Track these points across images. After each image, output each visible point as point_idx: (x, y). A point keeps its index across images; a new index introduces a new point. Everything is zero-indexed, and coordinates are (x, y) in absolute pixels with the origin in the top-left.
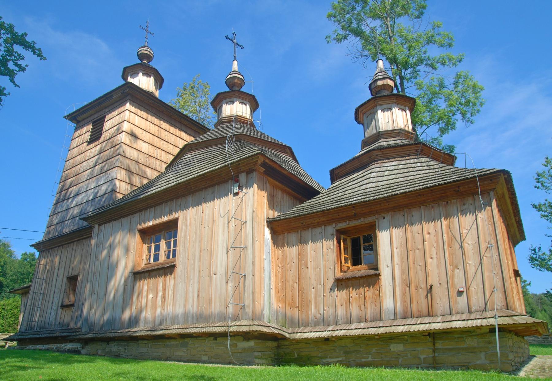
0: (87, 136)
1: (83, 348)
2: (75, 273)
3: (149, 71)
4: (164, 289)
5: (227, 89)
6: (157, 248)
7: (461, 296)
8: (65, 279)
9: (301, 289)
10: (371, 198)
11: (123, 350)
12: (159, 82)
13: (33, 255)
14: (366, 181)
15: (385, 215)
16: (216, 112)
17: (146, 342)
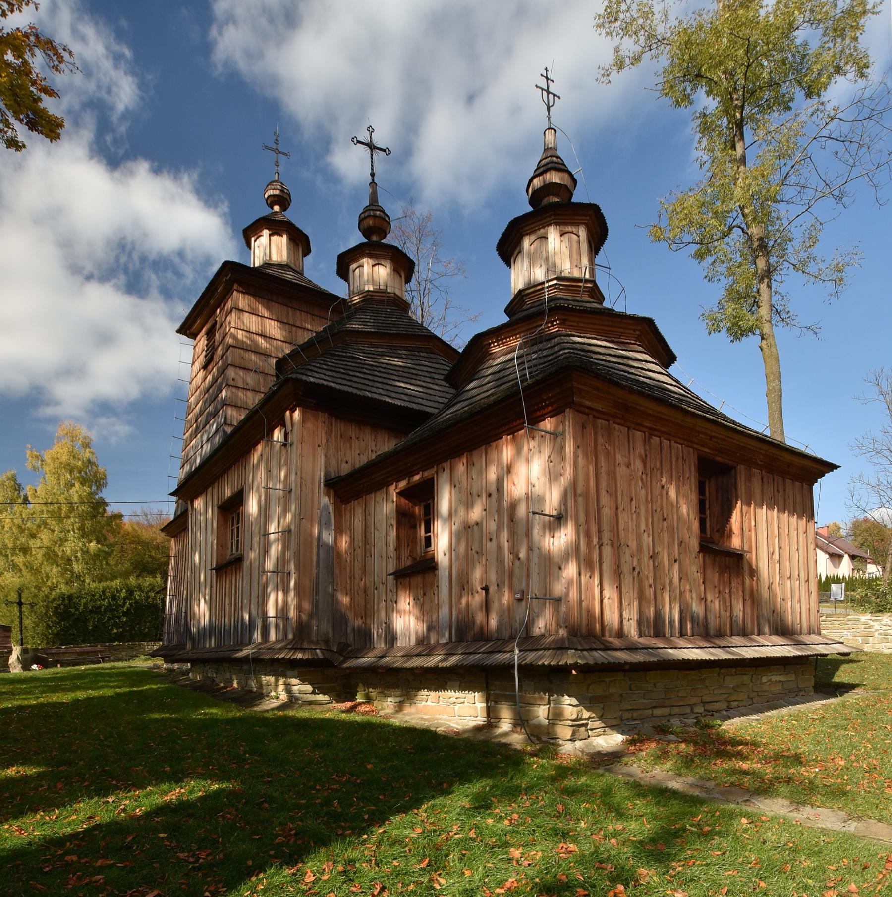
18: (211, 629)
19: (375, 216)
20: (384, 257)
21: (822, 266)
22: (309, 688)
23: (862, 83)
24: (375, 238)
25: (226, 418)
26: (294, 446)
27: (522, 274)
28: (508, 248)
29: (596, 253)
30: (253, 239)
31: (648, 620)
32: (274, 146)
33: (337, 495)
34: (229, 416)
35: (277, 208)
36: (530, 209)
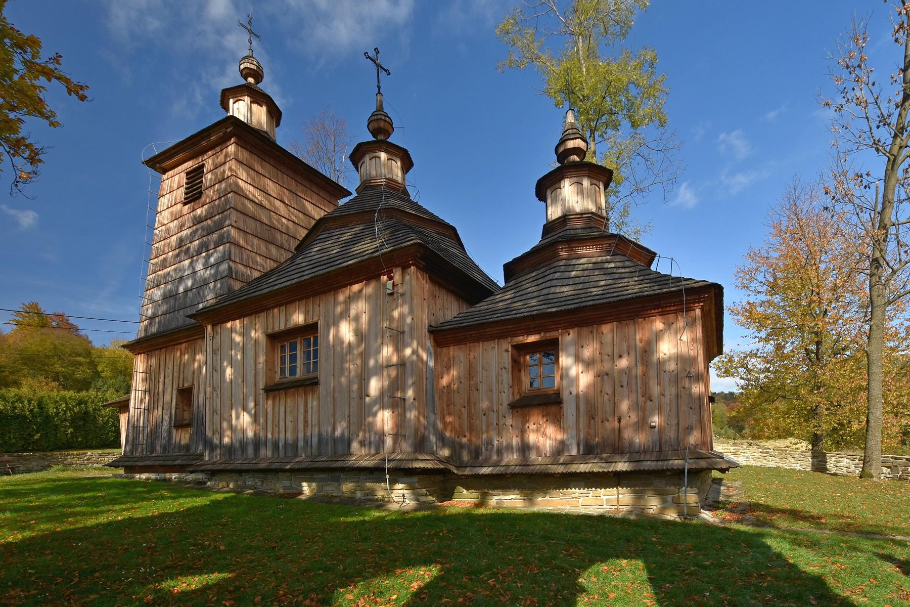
0: (180, 194)
1: (209, 480)
3: (259, 97)
4: (306, 412)
5: (370, 138)
6: (293, 358)
8: (175, 392)
9: (470, 417)
12: (275, 114)
14: (548, 284)
17: (288, 474)
18: (257, 443)
19: (385, 121)
20: (396, 156)
21: (629, 229)
23: (661, 130)
24: (381, 137)
28: (546, 187)
29: (407, 171)
30: (231, 101)
33: (435, 340)
36: (558, 165)
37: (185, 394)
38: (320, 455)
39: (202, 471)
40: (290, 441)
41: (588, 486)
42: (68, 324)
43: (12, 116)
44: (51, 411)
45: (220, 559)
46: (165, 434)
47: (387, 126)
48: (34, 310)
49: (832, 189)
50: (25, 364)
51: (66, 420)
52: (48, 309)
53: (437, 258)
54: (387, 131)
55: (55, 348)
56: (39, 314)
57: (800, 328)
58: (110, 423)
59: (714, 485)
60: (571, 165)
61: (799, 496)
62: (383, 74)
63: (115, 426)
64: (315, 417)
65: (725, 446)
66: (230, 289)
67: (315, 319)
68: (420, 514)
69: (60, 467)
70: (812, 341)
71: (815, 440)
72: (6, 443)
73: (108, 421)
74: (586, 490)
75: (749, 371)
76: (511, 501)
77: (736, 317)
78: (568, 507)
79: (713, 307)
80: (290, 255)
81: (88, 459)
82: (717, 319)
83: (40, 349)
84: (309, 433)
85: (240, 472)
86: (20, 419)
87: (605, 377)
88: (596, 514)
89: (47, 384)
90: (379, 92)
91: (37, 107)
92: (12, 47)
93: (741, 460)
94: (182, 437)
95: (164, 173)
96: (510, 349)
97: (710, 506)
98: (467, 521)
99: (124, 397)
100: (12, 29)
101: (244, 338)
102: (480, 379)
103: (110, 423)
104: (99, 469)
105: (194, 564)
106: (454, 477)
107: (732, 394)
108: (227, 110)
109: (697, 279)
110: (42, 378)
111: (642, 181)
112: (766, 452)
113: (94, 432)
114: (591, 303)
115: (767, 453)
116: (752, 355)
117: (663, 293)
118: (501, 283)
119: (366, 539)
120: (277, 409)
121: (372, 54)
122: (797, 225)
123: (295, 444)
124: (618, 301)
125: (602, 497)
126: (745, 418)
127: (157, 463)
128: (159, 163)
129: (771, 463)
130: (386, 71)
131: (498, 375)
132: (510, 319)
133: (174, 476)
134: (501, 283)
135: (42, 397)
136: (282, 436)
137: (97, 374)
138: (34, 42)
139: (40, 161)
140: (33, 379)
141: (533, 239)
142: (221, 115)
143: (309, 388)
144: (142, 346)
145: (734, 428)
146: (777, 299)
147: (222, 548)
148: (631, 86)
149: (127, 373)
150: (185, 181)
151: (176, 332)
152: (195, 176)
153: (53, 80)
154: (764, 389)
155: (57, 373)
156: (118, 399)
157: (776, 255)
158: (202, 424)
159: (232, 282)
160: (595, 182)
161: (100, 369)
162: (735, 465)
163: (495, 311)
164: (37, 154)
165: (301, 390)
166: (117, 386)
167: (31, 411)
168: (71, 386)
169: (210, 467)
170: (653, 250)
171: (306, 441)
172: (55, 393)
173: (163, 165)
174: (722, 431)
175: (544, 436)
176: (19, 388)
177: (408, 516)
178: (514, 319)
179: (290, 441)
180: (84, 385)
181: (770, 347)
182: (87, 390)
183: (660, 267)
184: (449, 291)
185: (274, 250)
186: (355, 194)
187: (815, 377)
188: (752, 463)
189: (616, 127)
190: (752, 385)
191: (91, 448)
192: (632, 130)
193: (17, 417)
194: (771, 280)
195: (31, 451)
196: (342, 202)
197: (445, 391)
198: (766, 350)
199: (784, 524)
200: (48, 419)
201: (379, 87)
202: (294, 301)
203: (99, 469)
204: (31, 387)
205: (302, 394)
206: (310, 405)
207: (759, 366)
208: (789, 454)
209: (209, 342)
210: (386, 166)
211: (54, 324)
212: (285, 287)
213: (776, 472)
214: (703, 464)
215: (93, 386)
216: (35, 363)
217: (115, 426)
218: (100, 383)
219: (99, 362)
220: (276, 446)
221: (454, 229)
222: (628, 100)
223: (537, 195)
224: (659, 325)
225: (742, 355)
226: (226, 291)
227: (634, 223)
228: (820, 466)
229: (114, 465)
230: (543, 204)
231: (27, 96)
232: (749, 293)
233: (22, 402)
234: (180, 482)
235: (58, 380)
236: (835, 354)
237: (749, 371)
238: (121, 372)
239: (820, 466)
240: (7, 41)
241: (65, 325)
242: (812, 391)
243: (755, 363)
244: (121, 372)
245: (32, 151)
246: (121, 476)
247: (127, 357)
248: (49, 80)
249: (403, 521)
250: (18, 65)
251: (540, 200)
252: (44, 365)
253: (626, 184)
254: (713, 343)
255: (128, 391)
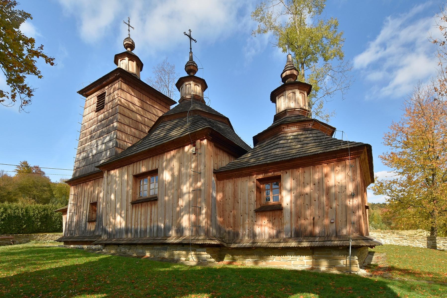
0: (94, 106)
1: (104, 249)
2: (95, 200)
3: (133, 58)
4: (151, 214)
5: (186, 75)
7: (332, 224)
8: (89, 204)
10: (279, 160)
11: (128, 251)
12: (140, 65)
13: (345, 188)
15: (288, 171)
16: (179, 91)
17: (142, 246)
18: (127, 230)
19: (194, 66)
22: (209, 256)
23: (341, 61)
24: (192, 74)
25: (117, 136)
26: (203, 155)
27: (283, 103)
29: (204, 90)
30: (119, 60)
31: (161, 229)
32: (128, 23)
33: (217, 177)
34: (118, 135)
35: (129, 49)
37: (94, 205)
38: (157, 236)
39: (100, 244)
40: (143, 229)
41: (296, 254)
42: (40, 171)
43: (21, 75)
44: (31, 214)
45: (107, 287)
46: (83, 226)
47: (194, 68)
48: (25, 165)
49: (439, 88)
50: (20, 191)
51: (38, 218)
52: (31, 164)
53: (218, 133)
54: (194, 70)
55: (34, 183)
56: (27, 167)
57: (423, 167)
58: (58, 220)
59: (370, 256)
60: (290, 82)
61: (419, 262)
62: (193, 42)
63: (60, 222)
64: (156, 217)
65: (378, 234)
66: (116, 153)
67: (157, 167)
68: (199, 268)
69: (34, 241)
70: (429, 174)
71: (432, 230)
72: (10, 229)
73: (57, 219)
74: (295, 257)
75: (392, 191)
76: (248, 263)
77: (384, 161)
78: (286, 266)
79: (367, 157)
80: (145, 135)
81: (47, 238)
82: (369, 163)
83: (27, 183)
84: (152, 225)
85: (118, 245)
86: (17, 218)
87: (306, 196)
88: (300, 270)
89: (30, 201)
90: (191, 51)
91: (32, 69)
92: (23, 44)
93: (383, 241)
94: (92, 227)
95: (87, 97)
96: (255, 181)
97: (365, 266)
98: (231, 272)
99: (65, 207)
100: (23, 35)
101: (120, 179)
102: (239, 197)
103: (58, 220)
104: (52, 243)
105: (95, 289)
106: (225, 249)
107: (385, 204)
108: (117, 65)
109: (357, 142)
110: (27, 198)
111: (329, 89)
112: (402, 236)
113: (50, 224)
114: (298, 156)
115: (402, 237)
116: (394, 182)
117: (338, 150)
118: (252, 147)
119: (178, 280)
120: (137, 213)
121: (188, 33)
122: (420, 109)
123: (146, 231)
124: (313, 155)
125: (304, 260)
126: (391, 219)
127: (79, 240)
128: (85, 92)
129: (405, 243)
130: (194, 40)
131: (249, 195)
132: (256, 165)
133: (85, 247)
134: (252, 147)
135: (27, 207)
136: (139, 227)
137: (53, 195)
138: (32, 41)
139: (32, 95)
140: (23, 198)
141: (269, 122)
142: (115, 67)
143: (153, 202)
144: (76, 181)
145: (385, 223)
146: (408, 150)
147: (108, 282)
148: (324, 39)
149: (67, 195)
150: (97, 100)
151: (89, 174)
152: (101, 98)
153: (40, 57)
154: (401, 201)
155: (34, 195)
156: (62, 208)
157: (408, 126)
158: (101, 220)
159: (117, 149)
160: (302, 92)
161: (54, 193)
162: (380, 244)
163: (242, 164)
164: (31, 92)
165: (149, 203)
166: (62, 201)
167: (22, 214)
168: (41, 202)
169: (105, 242)
170: (334, 127)
171: (151, 230)
172: (33, 205)
173: (87, 93)
174: (379, 225)
175: (264, 229)
176: (17, 203)
177: (193, 268)
178: (257, 165)
179: (143, 229)
180: (46, 201)
181: (405, 178)
182: (48, 203)
183: (337, 136)
184: (224, 151)
185: (137, 132)
186: (178, 103)
187: (431, 194)
188: (394, 243)
189: (316, 61)
190: (395, 199)
191: (49, 232)
192: (325, 62)
193: (15, 217)
194: (406, 140)
195: (21, 233)
196: (172, 107)
197: (221, 203)
198: (402, 179)
199: (398, 277)
200: (30, 218)
201: (191, 49)
202: (147, 158)
203: (52, 243)
204: (22, 202)
205: (149, 205)
206: (153, 211)
207: (398, 188)
208: (416, 238)
209: (105, 179)
210: (194, 88)
211: (34, 171)
212: (143, 151)
213: (408, 249)
214: (364, 244)
215: (51, 201)
216: (24, 190)
217: (60, 222)
218: (54, 200)
219: (54, 190)
220: (136, 231)
221: (228, 119)
222: (322, 47)
223: (271, 100)
224: (326, 169)
225: (389, 182)
226: (114, 154)
227: (322, 112)
228: (432, 245)
229: (59, 241)
230: (274, 104)
231: (29, 65)
232: (392, 148)
233: (18, 210)
234: (89, 249)
235: (35, 199)
236: (444, 181)
237: (392, 191)
238: (64, 195)
239: (432, 245)
240: (21, 42)
241: (39, 173)
242: (430, 202)
243: (395, 187)
244: (64, 195)
245: (29, 91)
246: (62, 246)
247: (67, 187)
248: (38, 57)
249: (192, 271)
250: (25, 52)
251: (273, 102)
252: (29, 191)
253: (321, 91)
254: (368, 176)
255: (67, 204)
